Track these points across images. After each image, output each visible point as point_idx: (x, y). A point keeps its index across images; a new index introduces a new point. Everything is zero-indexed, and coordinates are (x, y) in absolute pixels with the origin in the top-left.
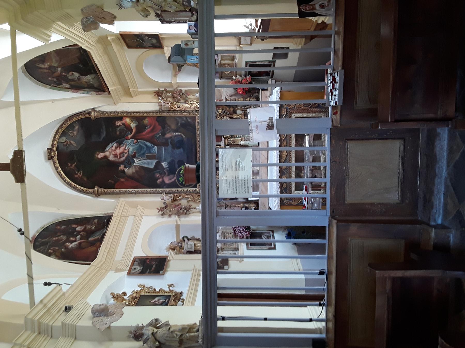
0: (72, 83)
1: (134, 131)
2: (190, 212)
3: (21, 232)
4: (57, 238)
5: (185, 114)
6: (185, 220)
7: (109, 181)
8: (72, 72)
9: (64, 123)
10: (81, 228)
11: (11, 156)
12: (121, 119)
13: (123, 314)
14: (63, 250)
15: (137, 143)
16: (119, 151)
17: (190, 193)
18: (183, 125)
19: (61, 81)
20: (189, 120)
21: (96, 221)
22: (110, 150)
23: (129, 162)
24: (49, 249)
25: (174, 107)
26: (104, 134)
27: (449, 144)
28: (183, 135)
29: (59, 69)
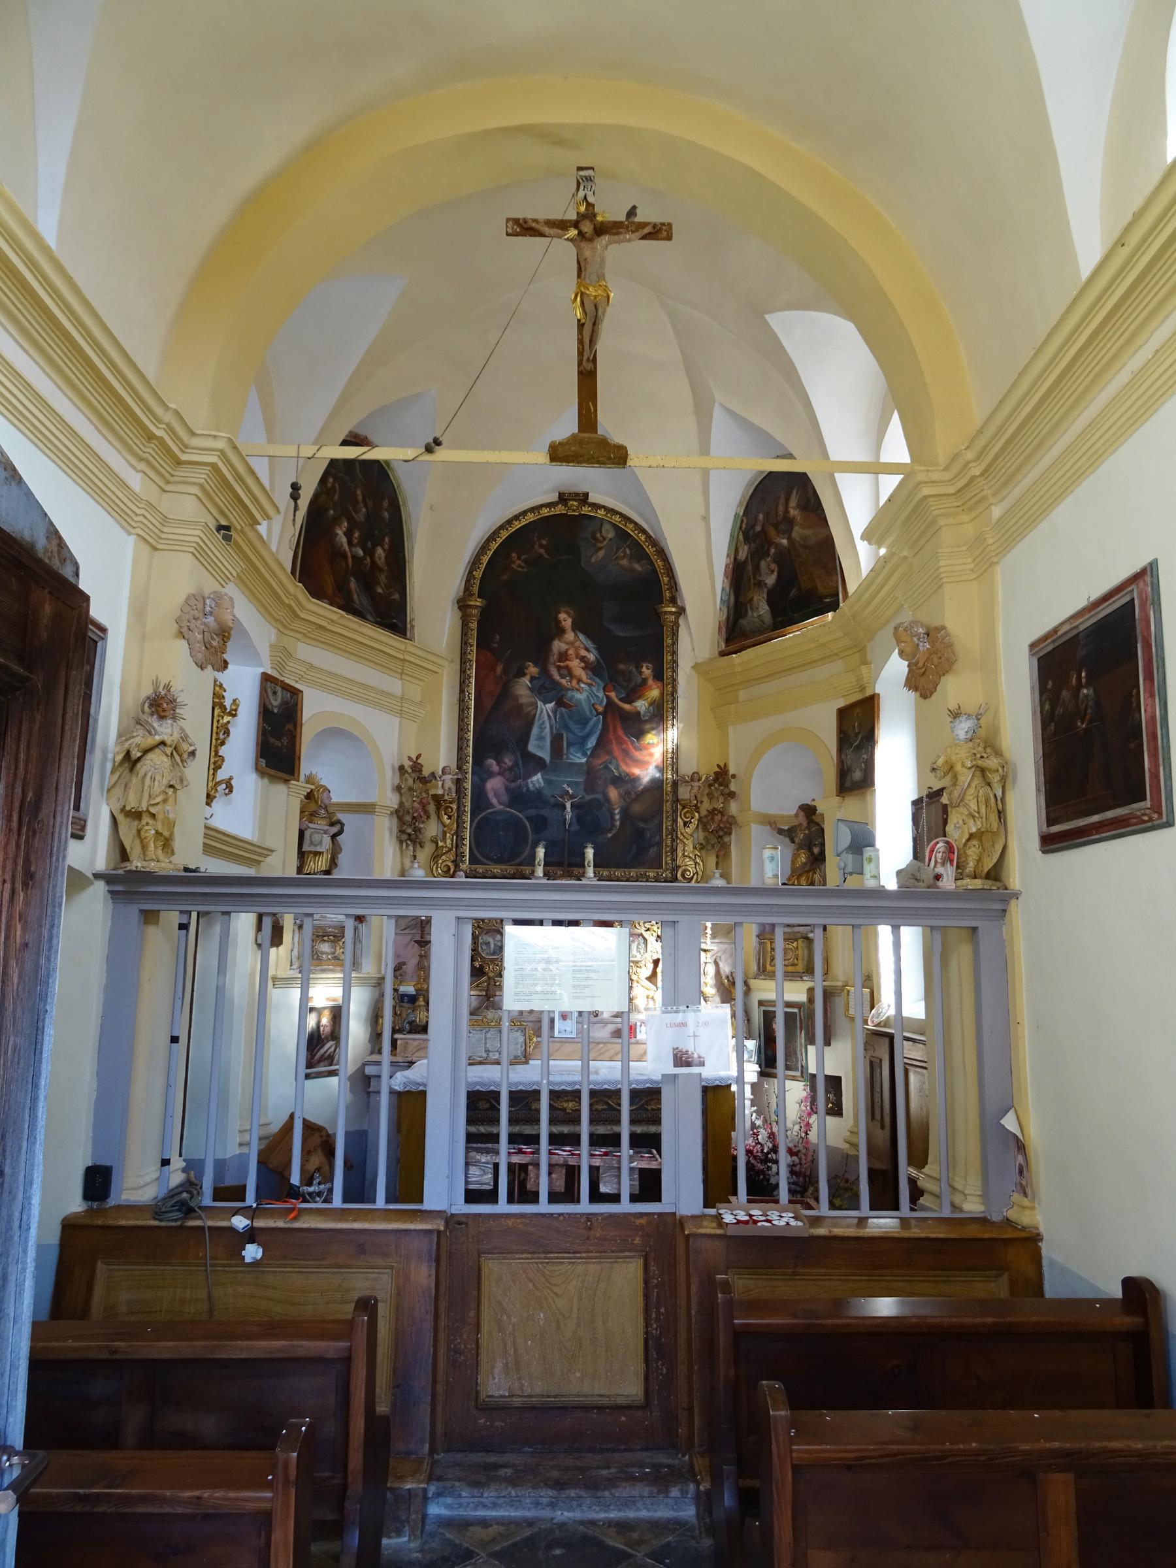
0: (750, 568)
1: (626, 707)
2: (404, 845)
3: (433, 445)
4: (360, 498)
5: (669, 842)
6: (384, 829)
7: (498, 637)
8: (776, 569)
9: (649, 537)
10: (380, 558)
11: (616, 438)
12: (659, 676)
13: (202, 669)
14: (332, 512)
15: (594, 711)
16: (575, 665)
17: (459, 845)
18: (639, 834)
19: (754, 543)
20: (653, 851)
21: (396, 596)
22: (577, 644)
23: (546, 688)
24: (335, 479)
25: (687, 812)
26: (620, 632)
27: (639, 1522)
28: (613, 832)
29: (785, 542)
